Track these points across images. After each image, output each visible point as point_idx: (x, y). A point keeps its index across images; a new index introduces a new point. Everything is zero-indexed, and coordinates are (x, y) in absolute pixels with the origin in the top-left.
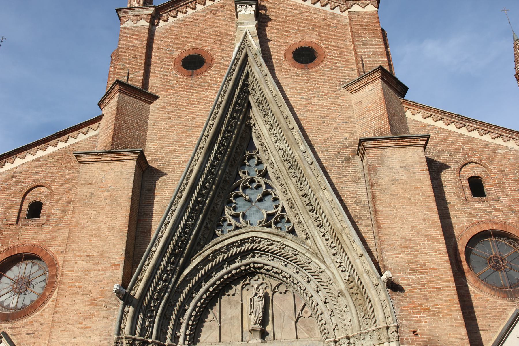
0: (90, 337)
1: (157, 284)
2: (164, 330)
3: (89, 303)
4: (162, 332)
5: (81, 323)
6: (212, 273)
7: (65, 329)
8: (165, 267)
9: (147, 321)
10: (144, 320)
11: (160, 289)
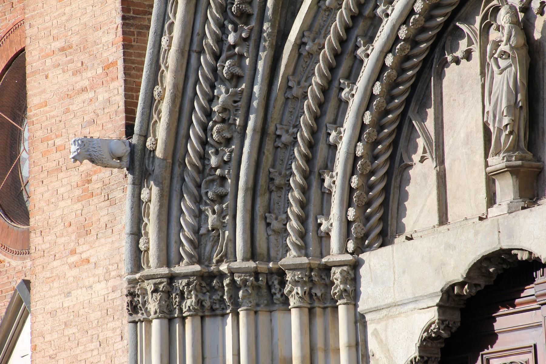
0: (91, 287)
1: (211, 100)
2: (276, 225)
3: (78, 192)
4: (270, 232)
5: (73, 252)
6: (376, 6)
7: (52, 273)
8: (220, 41)
9: (209, 213)
10: (199, 215)
11: (224, 109)
